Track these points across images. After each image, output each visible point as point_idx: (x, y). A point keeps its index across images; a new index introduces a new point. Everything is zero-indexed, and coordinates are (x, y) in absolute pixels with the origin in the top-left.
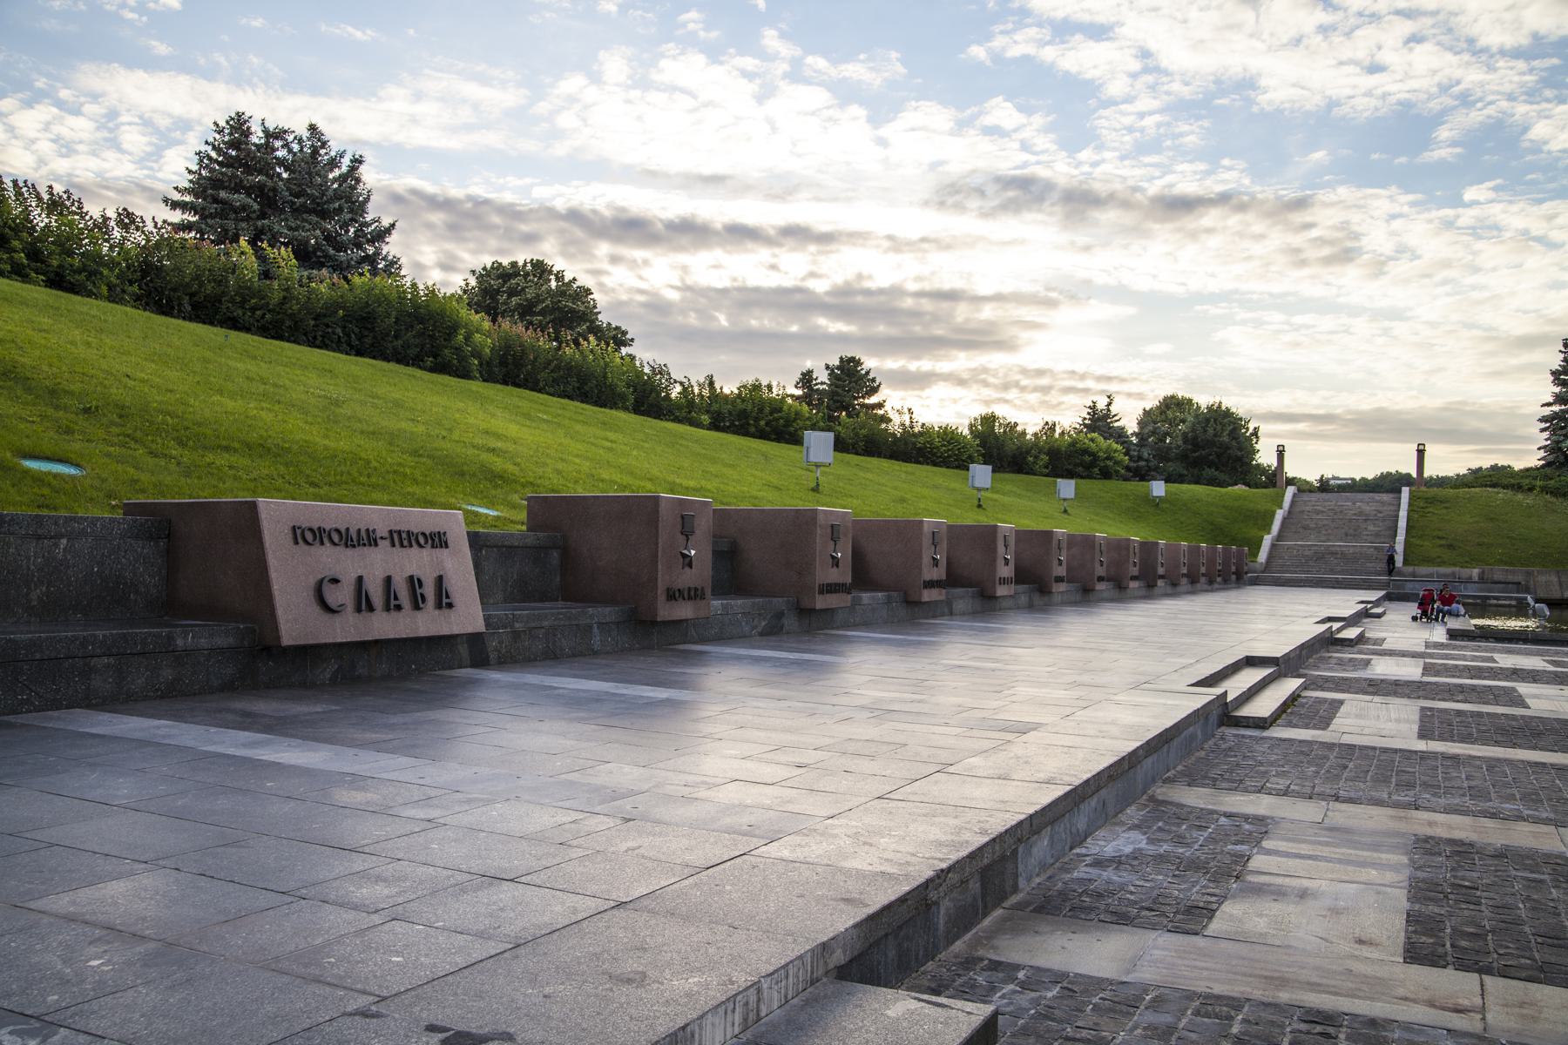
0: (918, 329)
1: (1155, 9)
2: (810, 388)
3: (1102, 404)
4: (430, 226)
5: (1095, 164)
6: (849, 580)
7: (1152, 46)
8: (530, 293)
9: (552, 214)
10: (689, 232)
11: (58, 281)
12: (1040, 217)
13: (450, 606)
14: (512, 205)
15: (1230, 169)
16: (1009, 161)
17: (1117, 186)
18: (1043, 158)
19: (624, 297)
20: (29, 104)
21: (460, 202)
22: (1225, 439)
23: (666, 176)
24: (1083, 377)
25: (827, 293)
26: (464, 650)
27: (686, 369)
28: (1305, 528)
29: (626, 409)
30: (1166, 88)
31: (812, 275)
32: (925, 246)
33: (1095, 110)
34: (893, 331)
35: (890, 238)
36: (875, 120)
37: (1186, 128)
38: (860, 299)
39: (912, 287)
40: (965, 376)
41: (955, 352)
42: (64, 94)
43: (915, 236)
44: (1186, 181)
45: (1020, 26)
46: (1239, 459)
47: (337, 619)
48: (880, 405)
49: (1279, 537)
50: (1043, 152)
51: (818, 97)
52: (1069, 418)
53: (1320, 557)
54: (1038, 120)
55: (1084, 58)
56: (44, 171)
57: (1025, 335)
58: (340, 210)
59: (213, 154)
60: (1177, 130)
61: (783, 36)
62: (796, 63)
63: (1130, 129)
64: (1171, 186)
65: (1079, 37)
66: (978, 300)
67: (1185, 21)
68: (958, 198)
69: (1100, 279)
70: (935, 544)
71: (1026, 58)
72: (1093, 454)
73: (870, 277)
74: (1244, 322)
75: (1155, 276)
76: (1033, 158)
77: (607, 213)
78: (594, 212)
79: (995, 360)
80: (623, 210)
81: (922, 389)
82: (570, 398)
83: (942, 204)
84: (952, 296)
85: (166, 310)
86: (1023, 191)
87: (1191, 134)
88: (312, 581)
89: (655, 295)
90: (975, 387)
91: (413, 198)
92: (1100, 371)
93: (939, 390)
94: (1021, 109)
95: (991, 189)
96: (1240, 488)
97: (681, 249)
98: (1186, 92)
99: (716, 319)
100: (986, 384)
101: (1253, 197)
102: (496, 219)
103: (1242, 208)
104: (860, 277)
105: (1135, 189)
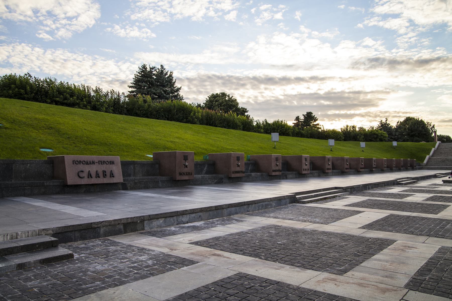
0: (349, 102)
1: (413, 7)
2: (299, 121)
3: (384, 121)
4: (218, 84)
5: (397, 53)
6: (281, 169)
7: (413, 18)
8: (220, 101)
9: (249, 78)
10: (285, 80)
11: (95, 108)
12: (382, 69)
13: (113, 177)
14: (238, 77)
15: (440, 50)
16: (372, 54)
17: (404, 59)
18: (382, 52)
19: (269, 99)
20: (124, 63)
21: (225, 77)
22: (420, 129)
23: (278, 66)
24: (398, 113)
25: (324, 94)
26: (120, 186)
27: (257, 117)
28: (441, 153)
29: (240, 129)
30: (417, 30)
31: (319, 89)
32: (350, 79)
33: (396, 38)
34: (343, 103)
35: (340, 78)
36: (333, 47)
37: (425, 40)
38: (333, 95)
39: (347, 91)
40: (364, 114)
41: (360, 108)
42: (132, 60)
43: (347, 77)
44: (426, 54)
45: (372, 17)
46: (425, 134)
47: (83, 179)
48: (318, 124)
49: (432, 156)
50: (382, 51)
51: (316, 42)
52: (376, 124)
53: (443, 161)
54: (379, 42)
55: (393, 24)
56: (127, 78)
57: (380, 102)
58: (168, 85)
59: (138, 74)
60: (422, 41)
61: (306, 27)
62: (310, 34)
63: (407, 42)
64: (421, 57)
65: (390, 18)
66: (366, 93)
67: (422, 10)
68: (358, 65)
69: (402, 85)
70: (306, 160)
71: (374, 26)
72: (377, 135)
73: (335, 89)
74: (447, 94)
75: (418, 83)
76: (379, 53)
77: (263, 77)
78: (260, 77)
79: (372, 110)
80: (267, 76)
81: (352, 119)
82: (225, 127)
83: (353, 68)
84: (359, 92)
85: (121, 113)
86: (376, 62)
87: (426, 41)
88: (77, 172)
89: (277, 97)
90: (367, 117)
91: (213, 77)
92: (403, 111)
93: (356, 119)
94: (373, 40)
95: (367, 62)
96: (423, 142)
97: (283, 85)
98: (424, 30)
99: (293, 103)
100: (370, 116)
101: (448, 57)
102: (234, 81)
103: (444, 61)
104: (332, 89)
105: (410, 59)
